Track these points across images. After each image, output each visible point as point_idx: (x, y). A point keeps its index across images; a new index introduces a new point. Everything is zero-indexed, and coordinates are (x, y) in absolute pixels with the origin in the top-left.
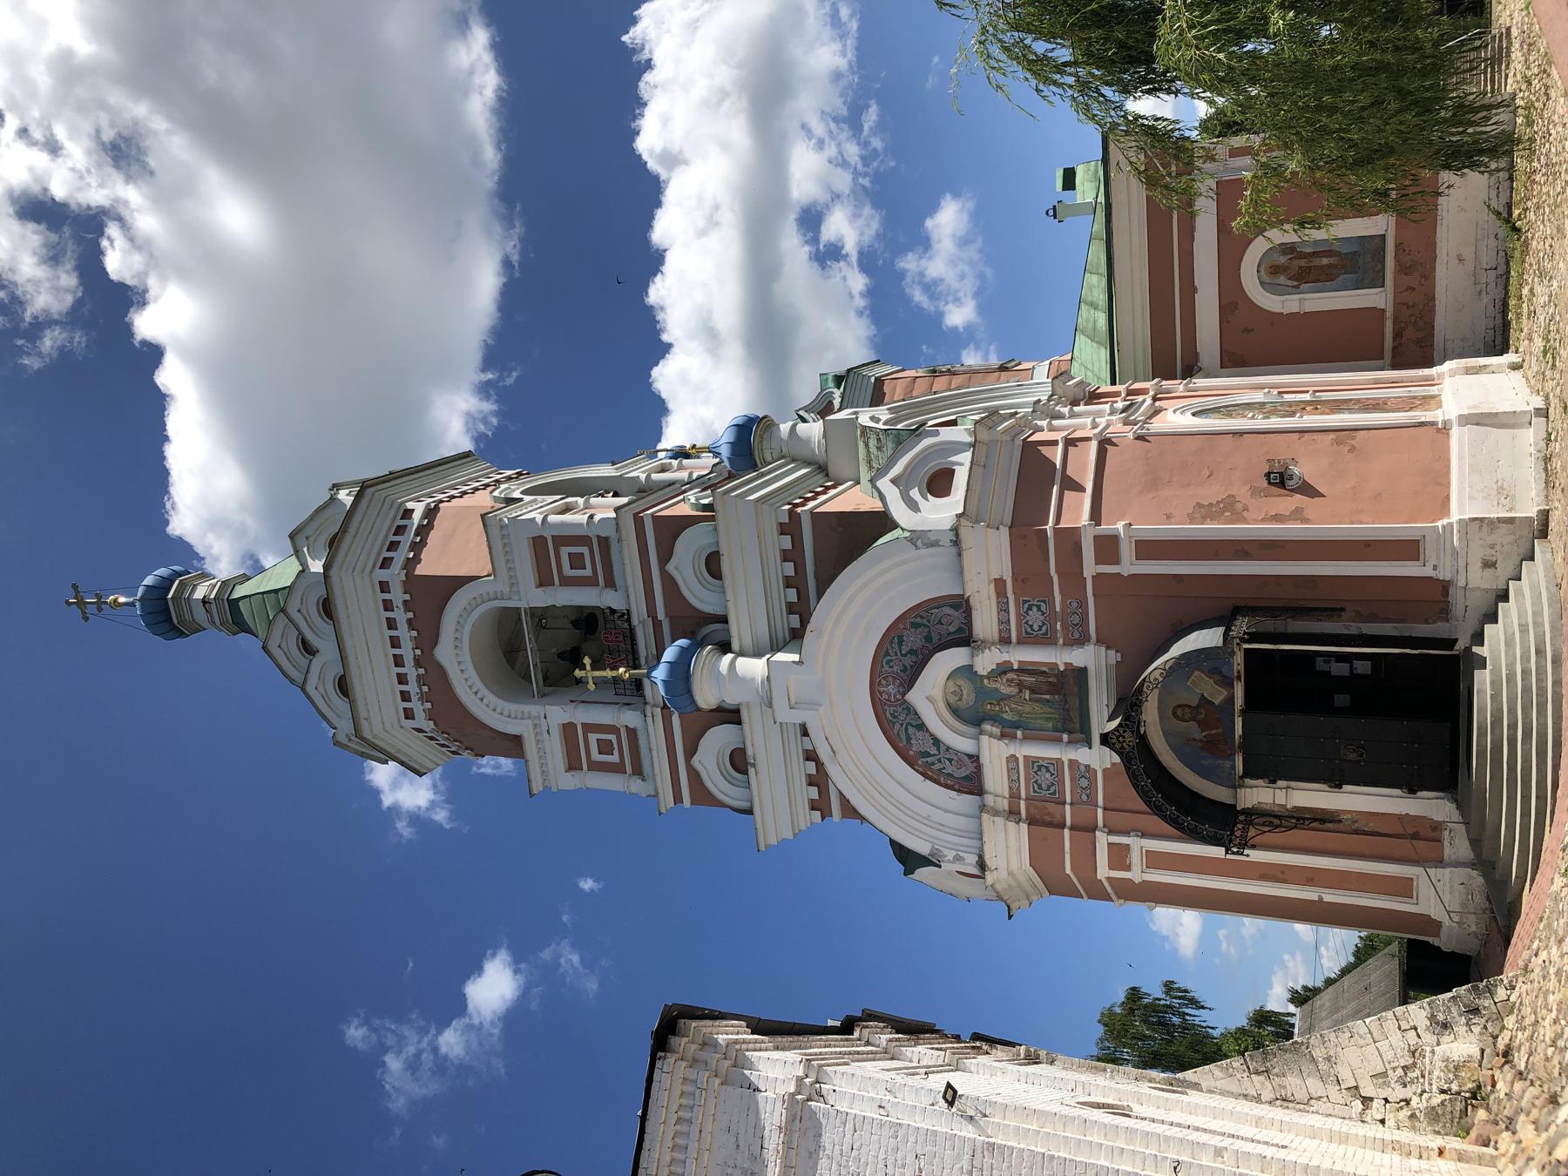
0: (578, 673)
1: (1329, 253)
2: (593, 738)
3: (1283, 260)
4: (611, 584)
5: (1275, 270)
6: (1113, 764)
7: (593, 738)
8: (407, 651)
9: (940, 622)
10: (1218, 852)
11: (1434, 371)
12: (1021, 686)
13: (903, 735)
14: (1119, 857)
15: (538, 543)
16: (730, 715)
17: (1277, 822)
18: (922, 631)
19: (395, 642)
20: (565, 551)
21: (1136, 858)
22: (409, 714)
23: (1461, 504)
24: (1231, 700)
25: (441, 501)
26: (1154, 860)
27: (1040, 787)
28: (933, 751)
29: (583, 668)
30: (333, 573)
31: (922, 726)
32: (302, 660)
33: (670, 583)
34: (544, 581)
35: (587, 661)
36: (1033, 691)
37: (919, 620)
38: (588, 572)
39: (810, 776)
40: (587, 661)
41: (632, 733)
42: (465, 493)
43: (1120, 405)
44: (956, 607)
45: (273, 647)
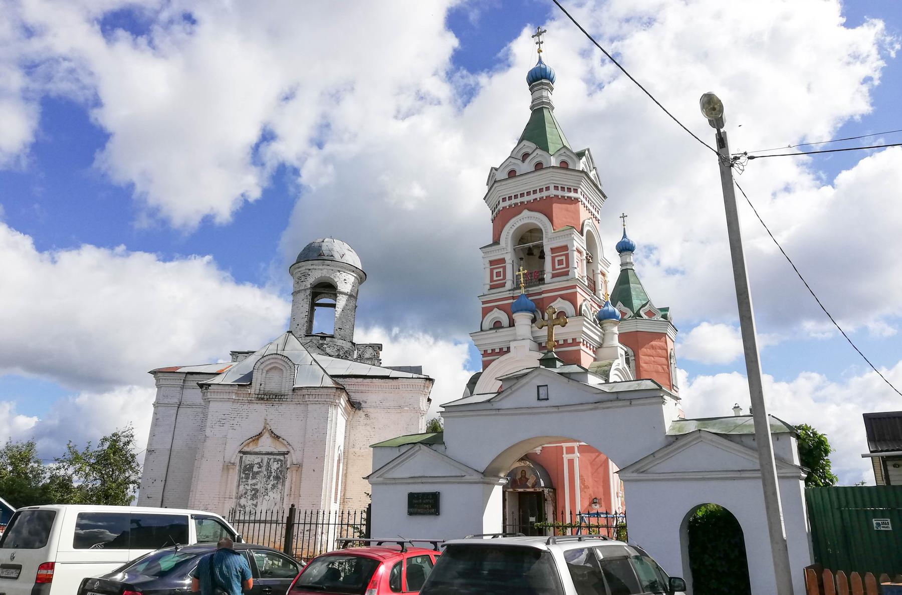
0: (521, 268)
2: (501, 270)
4: (554, 276)
7: (501, 270)
8: (526, 199)
15: (565, 248)
16: (512, 324)
19: (528, 193)
20: (564, 258)
21: (570, 456)
22: (504, 200)
24: (528, 487)
30: (551, 170)
33: (554, 299)
38: (557, 267)
41: (503, 285)
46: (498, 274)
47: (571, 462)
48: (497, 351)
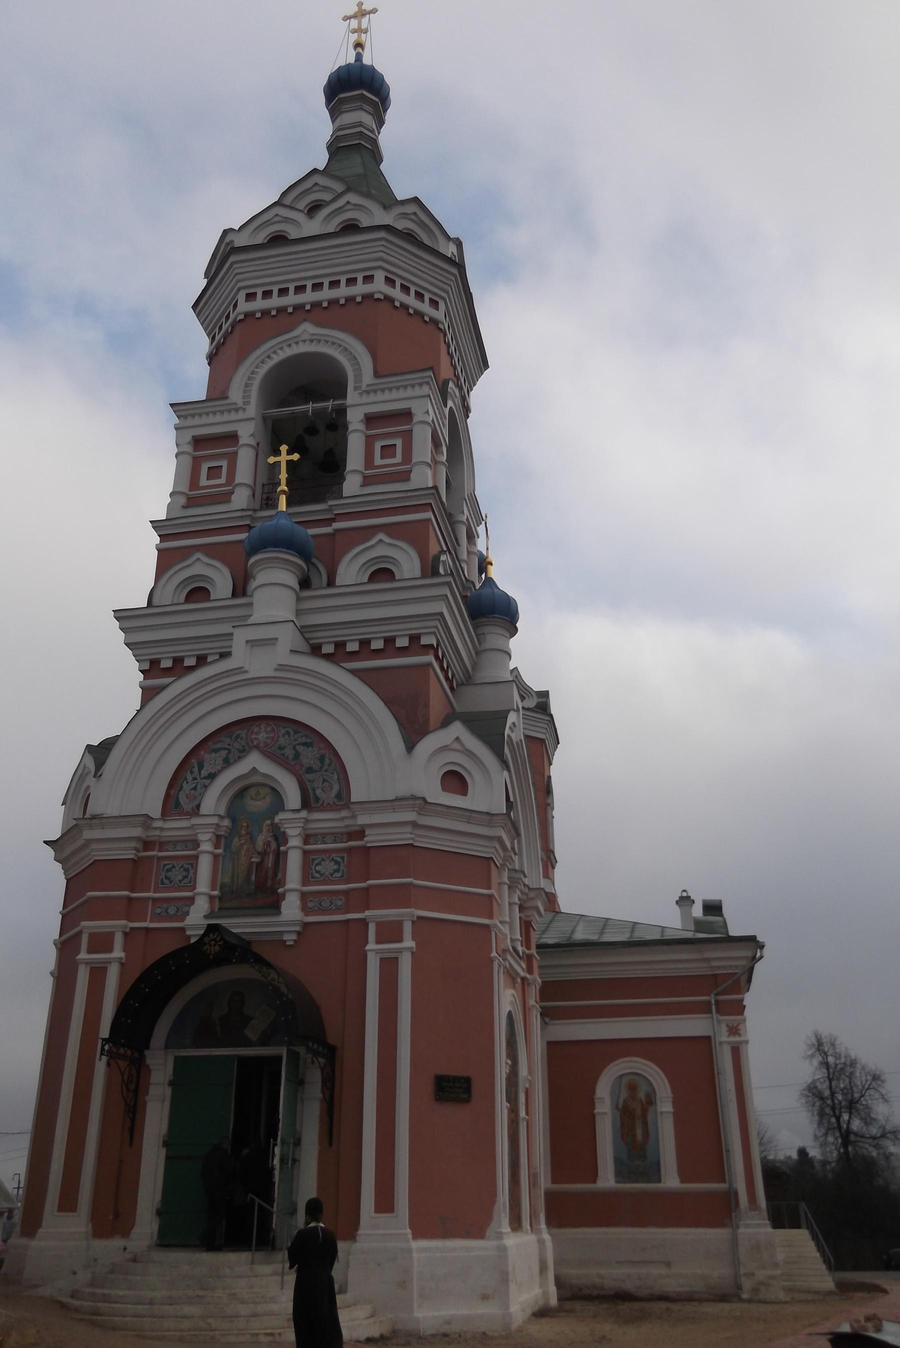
0: (284, 448)
1: (646, 1134)
3: (642, 1095)
5: (632, 1088)
6: (189, 937)
9: (325, 781)
10: (105, 1031)
11: (543, 1226)
12: (263, 854)
13: (219, 745)
14: (101, 943)
17: (132, 1087)
18: (316, 765)
22: (251, 297)
23: (424, 1250)
24: (248, 1044)
25: (445, 335)
26: (98, 973)
27: (169, 870)
28: (204, 773)
29: (289, 453)
31: (227, 763)
32: (302, 204)
34: (371, 420)
35: (296, 457)
36: (259, 865)
37: (327, 761)
39: (160, 662)
40: (296, 457)
41: (225, 498)
42: (452, 357)
43: (520, 949)
44: (338, 796)
45: (316, 179)
46: (214, 472)
47: (389, 966)
48: (166, 664)
